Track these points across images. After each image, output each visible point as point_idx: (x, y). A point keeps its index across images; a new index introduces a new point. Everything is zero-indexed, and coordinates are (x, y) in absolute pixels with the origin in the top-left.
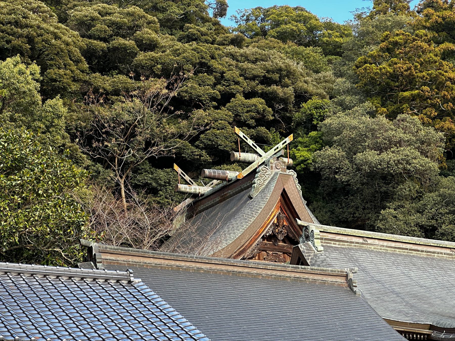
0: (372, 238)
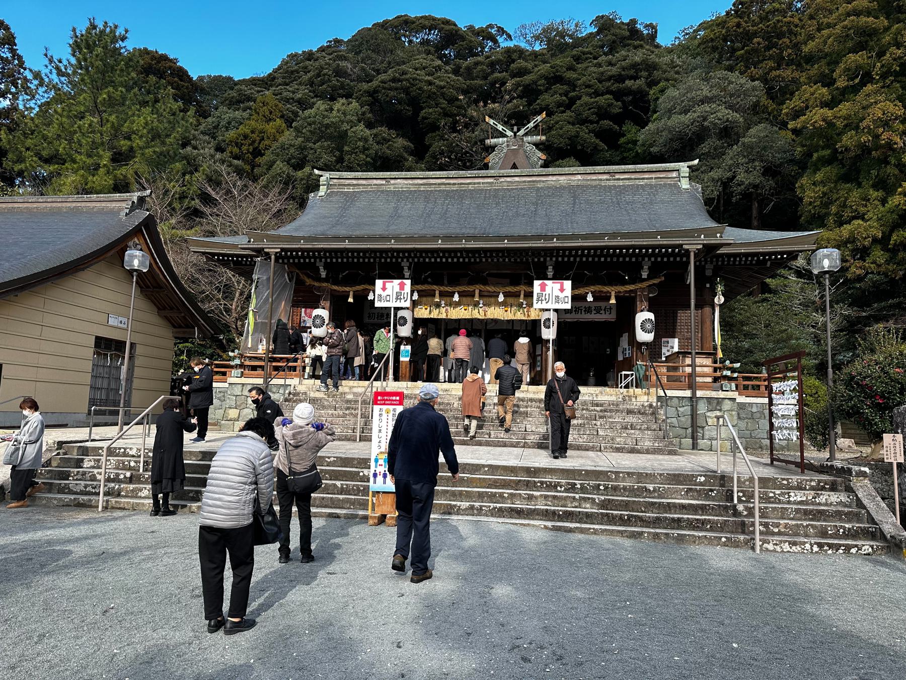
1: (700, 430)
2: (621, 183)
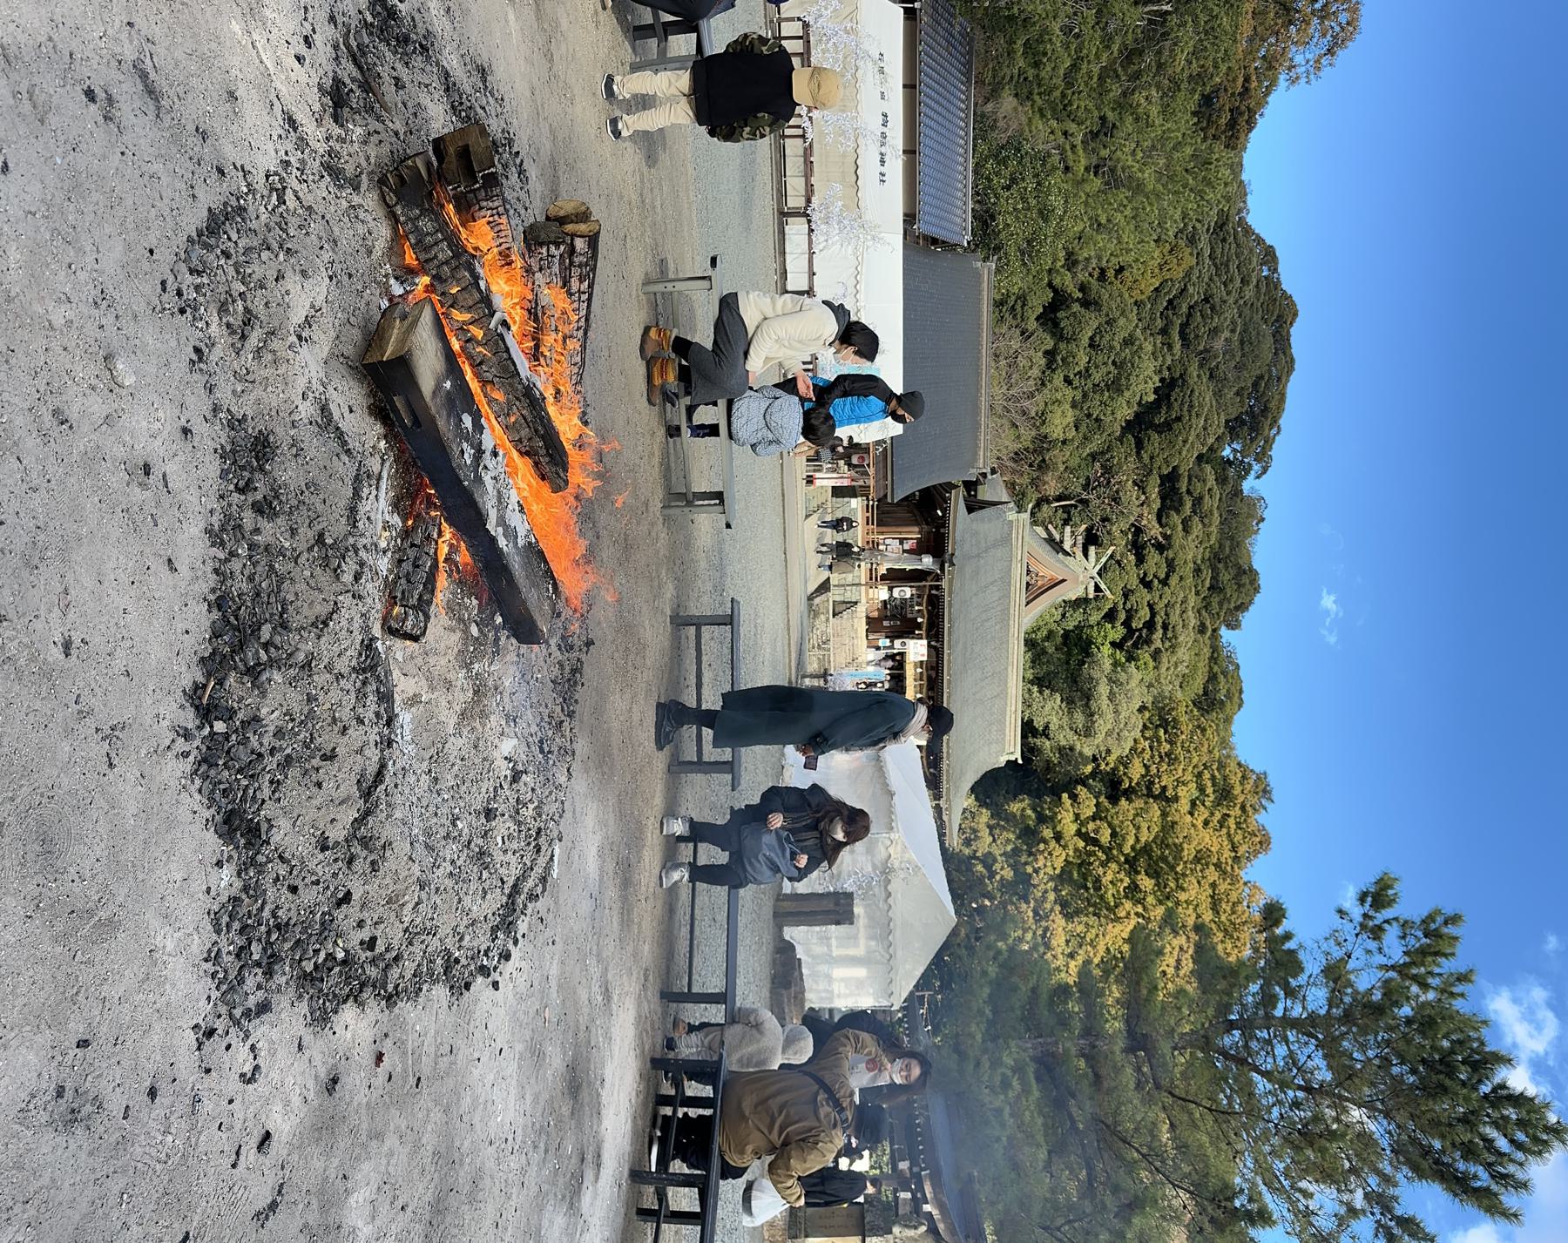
1: (705, 522)
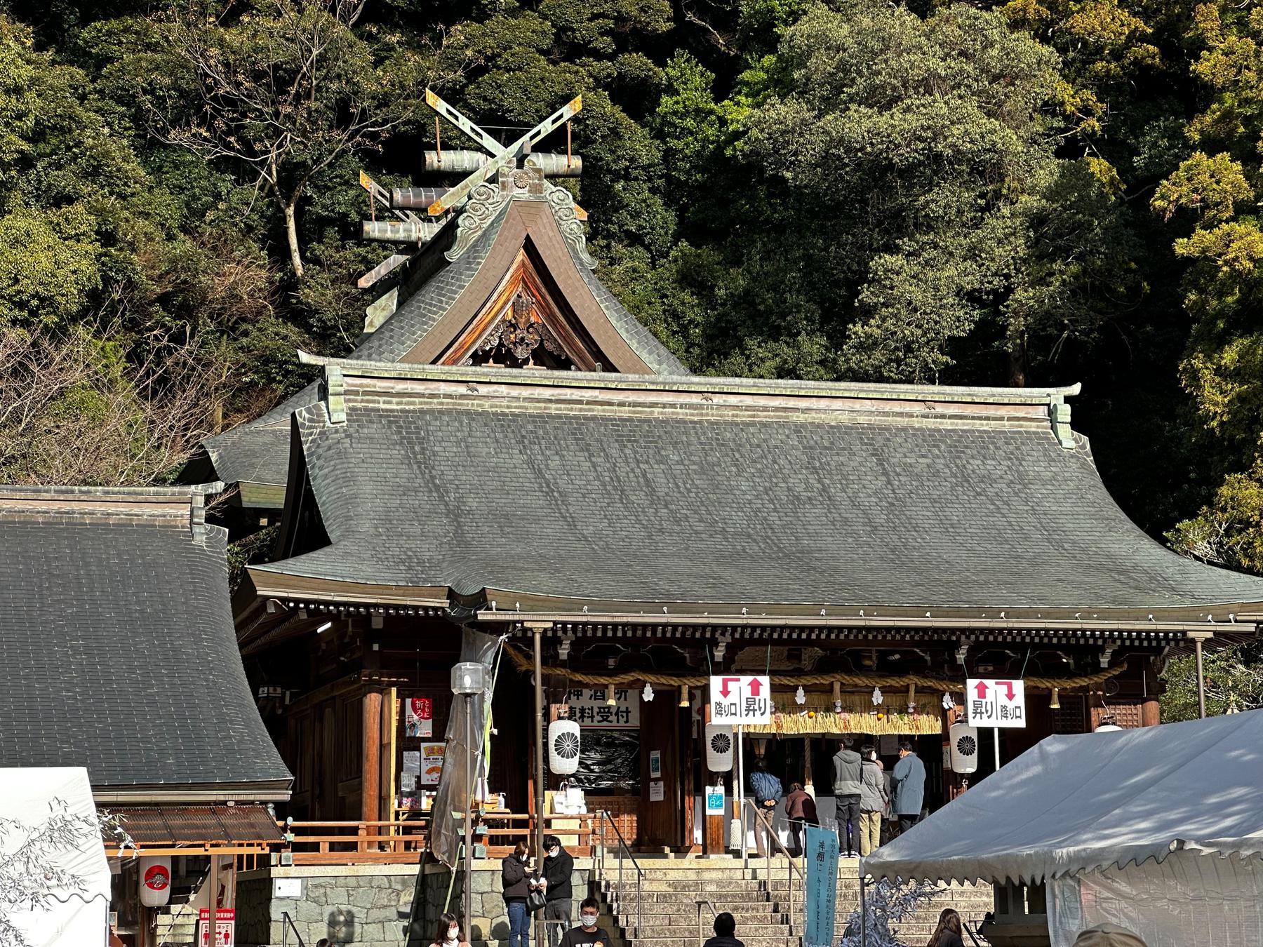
0: (490, 383)
2: (948, 424)
